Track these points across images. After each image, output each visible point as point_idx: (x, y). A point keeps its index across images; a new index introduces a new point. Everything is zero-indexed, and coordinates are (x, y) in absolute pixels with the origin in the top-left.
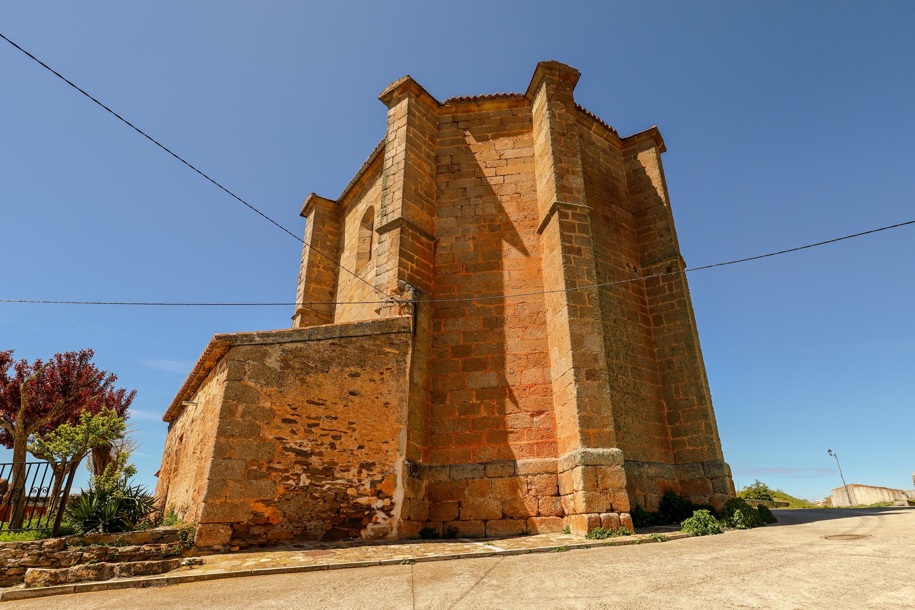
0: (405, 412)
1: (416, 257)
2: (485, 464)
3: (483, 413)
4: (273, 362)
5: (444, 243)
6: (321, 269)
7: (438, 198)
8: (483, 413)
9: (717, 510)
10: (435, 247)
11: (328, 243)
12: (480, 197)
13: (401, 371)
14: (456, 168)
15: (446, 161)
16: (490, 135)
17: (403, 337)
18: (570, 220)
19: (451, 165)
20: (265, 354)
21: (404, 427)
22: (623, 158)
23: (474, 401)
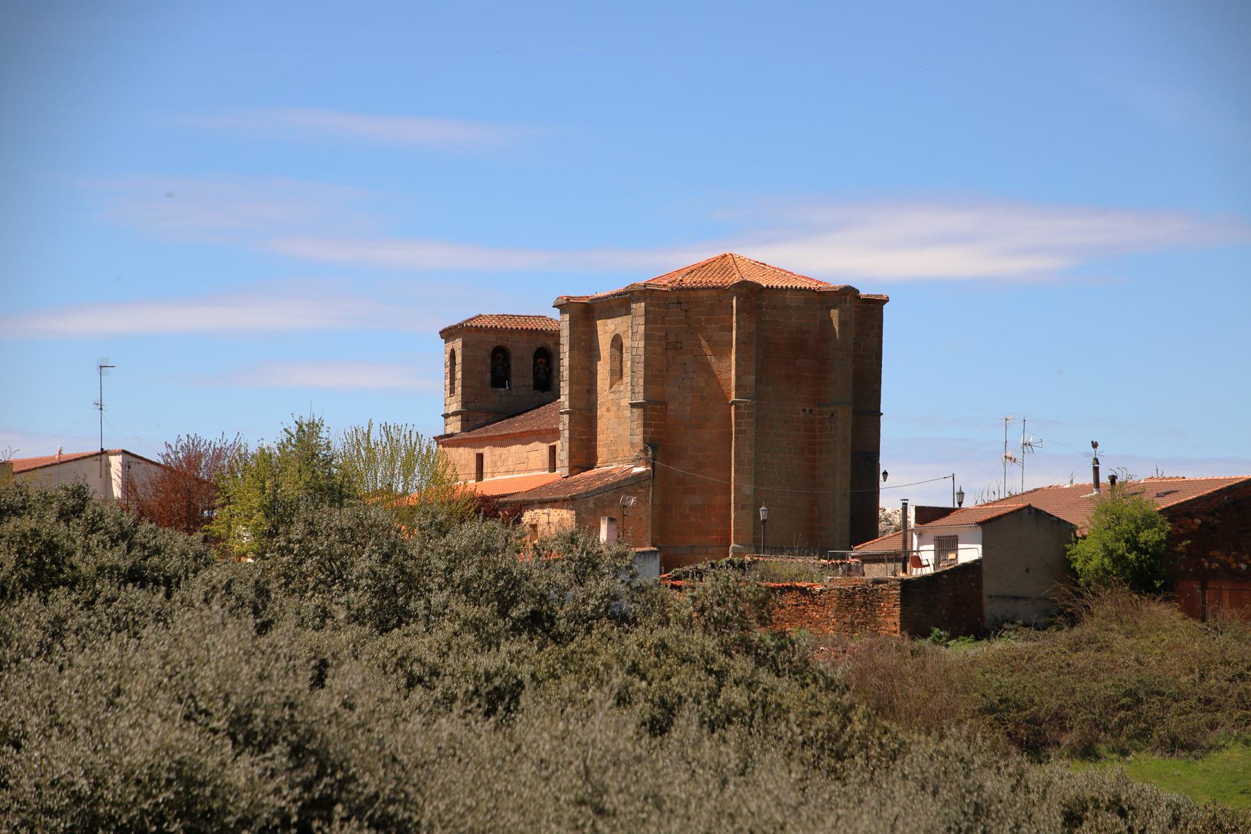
0: (650, 521)
1: (653, 423)
2: (692, 547)
3: (693, 519)
4: (591, 505)
5: (671, 407)
6: (579, 371)
7: (667, 370)
8: (693, 519)
9: (338, 446)
10: (666, 409)
11: (583, 344)
12: (695, 372)
13: (647, 501)
14: (679, 345)
15: (672, 339)
16: (703, 318)
17: (647, 482)
18: (742, 410)
19: (560, 699)
20: (588, 502)
21: (649, 530)
22: (818, 305)
23: (688, 512)
